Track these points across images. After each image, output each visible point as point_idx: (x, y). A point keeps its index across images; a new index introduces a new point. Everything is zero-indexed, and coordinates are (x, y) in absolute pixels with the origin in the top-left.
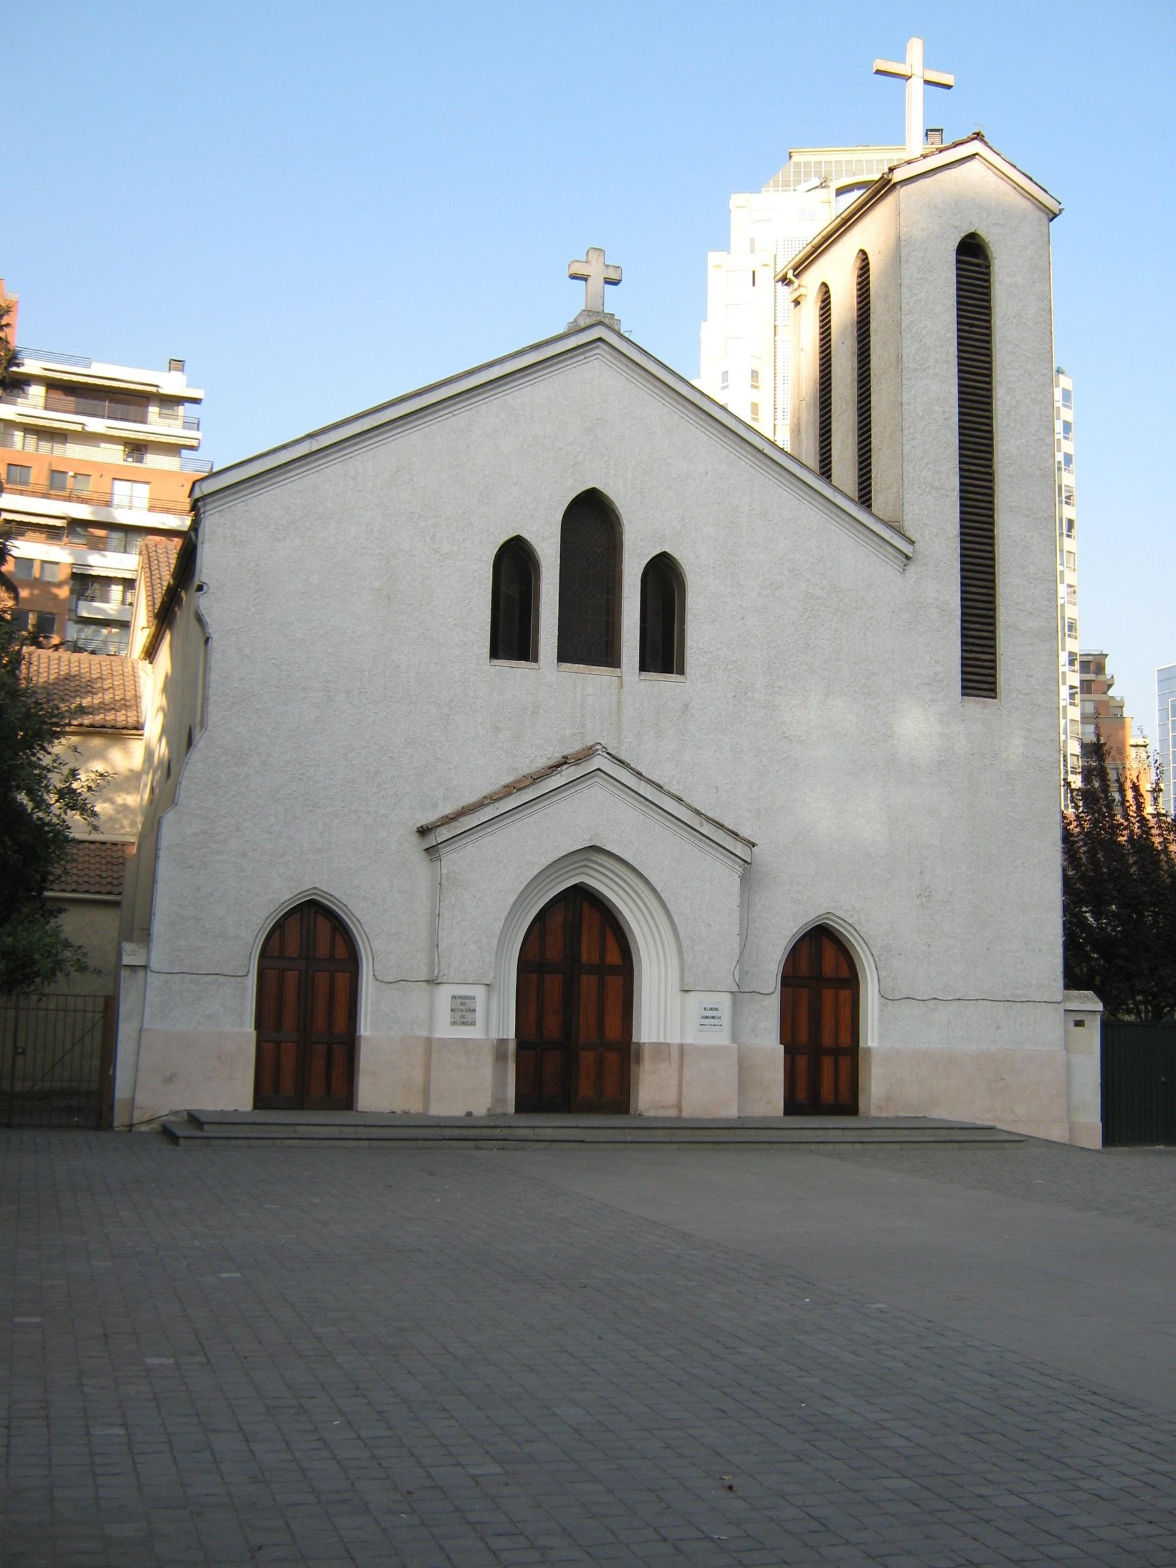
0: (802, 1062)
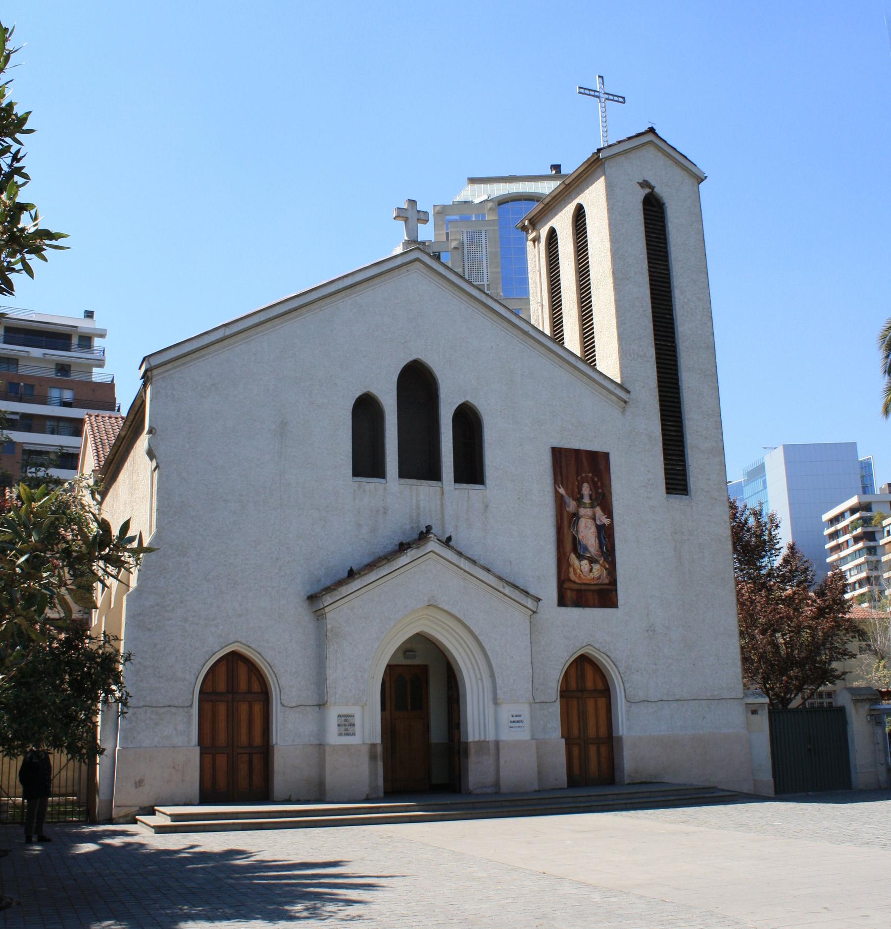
0: (576, 751)
